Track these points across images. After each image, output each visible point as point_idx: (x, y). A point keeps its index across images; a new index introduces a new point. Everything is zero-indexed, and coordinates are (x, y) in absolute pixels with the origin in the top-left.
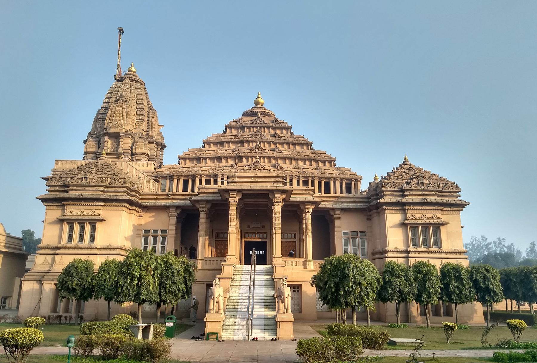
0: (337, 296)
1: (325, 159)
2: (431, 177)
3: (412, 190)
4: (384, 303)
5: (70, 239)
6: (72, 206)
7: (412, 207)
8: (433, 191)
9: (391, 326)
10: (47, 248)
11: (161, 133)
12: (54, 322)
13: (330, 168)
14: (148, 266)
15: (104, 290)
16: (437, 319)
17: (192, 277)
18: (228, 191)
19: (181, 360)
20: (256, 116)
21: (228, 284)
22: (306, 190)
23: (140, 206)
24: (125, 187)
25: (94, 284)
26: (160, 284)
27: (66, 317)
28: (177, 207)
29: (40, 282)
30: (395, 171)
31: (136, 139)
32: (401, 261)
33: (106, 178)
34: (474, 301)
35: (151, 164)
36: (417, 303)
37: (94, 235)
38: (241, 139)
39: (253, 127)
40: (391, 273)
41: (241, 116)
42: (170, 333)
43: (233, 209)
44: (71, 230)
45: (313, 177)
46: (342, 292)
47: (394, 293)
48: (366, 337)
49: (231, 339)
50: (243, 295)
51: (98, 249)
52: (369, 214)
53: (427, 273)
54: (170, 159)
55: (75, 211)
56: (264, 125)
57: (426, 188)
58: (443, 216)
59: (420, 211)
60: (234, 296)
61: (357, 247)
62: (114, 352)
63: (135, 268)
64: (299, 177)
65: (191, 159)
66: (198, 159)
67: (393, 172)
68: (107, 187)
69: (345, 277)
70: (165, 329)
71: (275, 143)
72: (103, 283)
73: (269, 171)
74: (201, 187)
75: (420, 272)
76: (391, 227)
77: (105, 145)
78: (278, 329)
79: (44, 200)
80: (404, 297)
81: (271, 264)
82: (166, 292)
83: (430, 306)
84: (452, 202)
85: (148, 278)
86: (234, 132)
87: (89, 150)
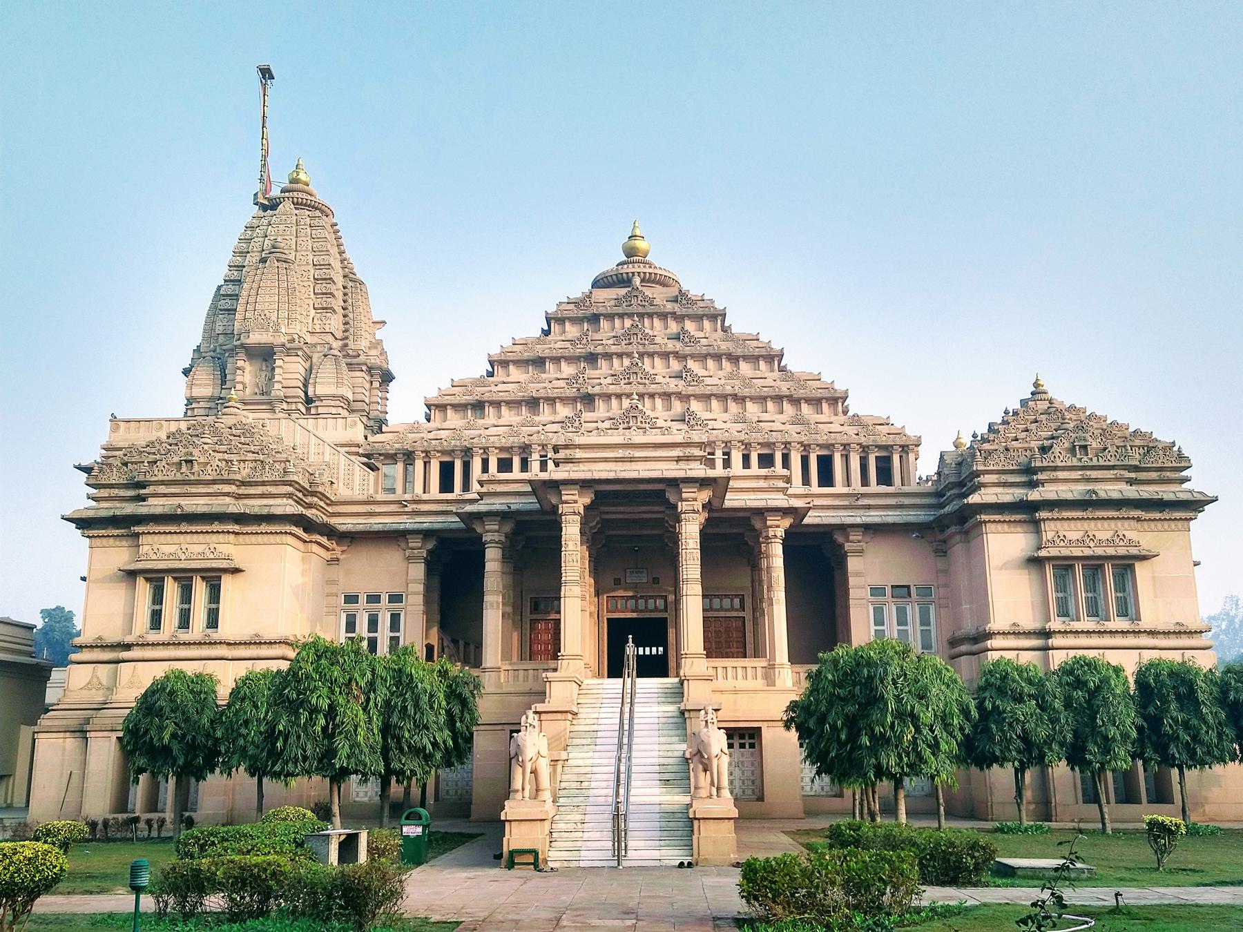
1: (819, 394)
2: (1109, 430)
3: (1055, 469)
4: (982, 769)
5: (156, 621)
6: (156, 537)
7: (1056, 514)
8: (1113, 467)
10: (97, 647)
11: (380, 342)
12: (119, 836)
13: (833, 419)
14: (350, 680)
15: (244, 749)
16: (1129, 809)
17: (471, 712)
19: (435, 918)
20: (629, 288)
21: (562, 725)
22: (766, 478)
24: (289, 483)
25: (219, 734)
26: (386, 729)
27: (149, 822)
28: (427, 534)
29: (82, 732)
30: (1010, 419)
32: (1026, 658)
34: (1233, 760)
35: (355, 423)
36: (1072, 769)
37: (218, 609)
38: (591, 348)
39: (622, 316)
41: (587, 287)
42: (416, 854)
43: (571, 531)
44: (158, 598)
46: (865, 740)
47: (1009, 741)
49: (573, 864)
51: (229, 644)
52: (940, 537)
54: (404, 409)
55: (163, 549)
56: (650, 309)
57: (1095, 462)
58: (1139, 535)
59: (1079, 523)
60: (578, 757)
61: (909, 628)
62: (260, 902)
64: (747, 445)
65: (459, 407)
66: (479, 406)
67: (1005, 422)
68: (243, 483)
69: (874, 701)
70: (400, 842)
73: (665, 430)
74: (485, 477)
75: (1080, 684)
76: (1004, 567)
77: (239, 379)
78: (695, 837)
80: (1035, 753)
81: (678, 675)
82: (401, 750)
83: (1109, 775)
84: (1166, 497)
85: (352, 711)
86: (572, 331)
87: (197, 392)
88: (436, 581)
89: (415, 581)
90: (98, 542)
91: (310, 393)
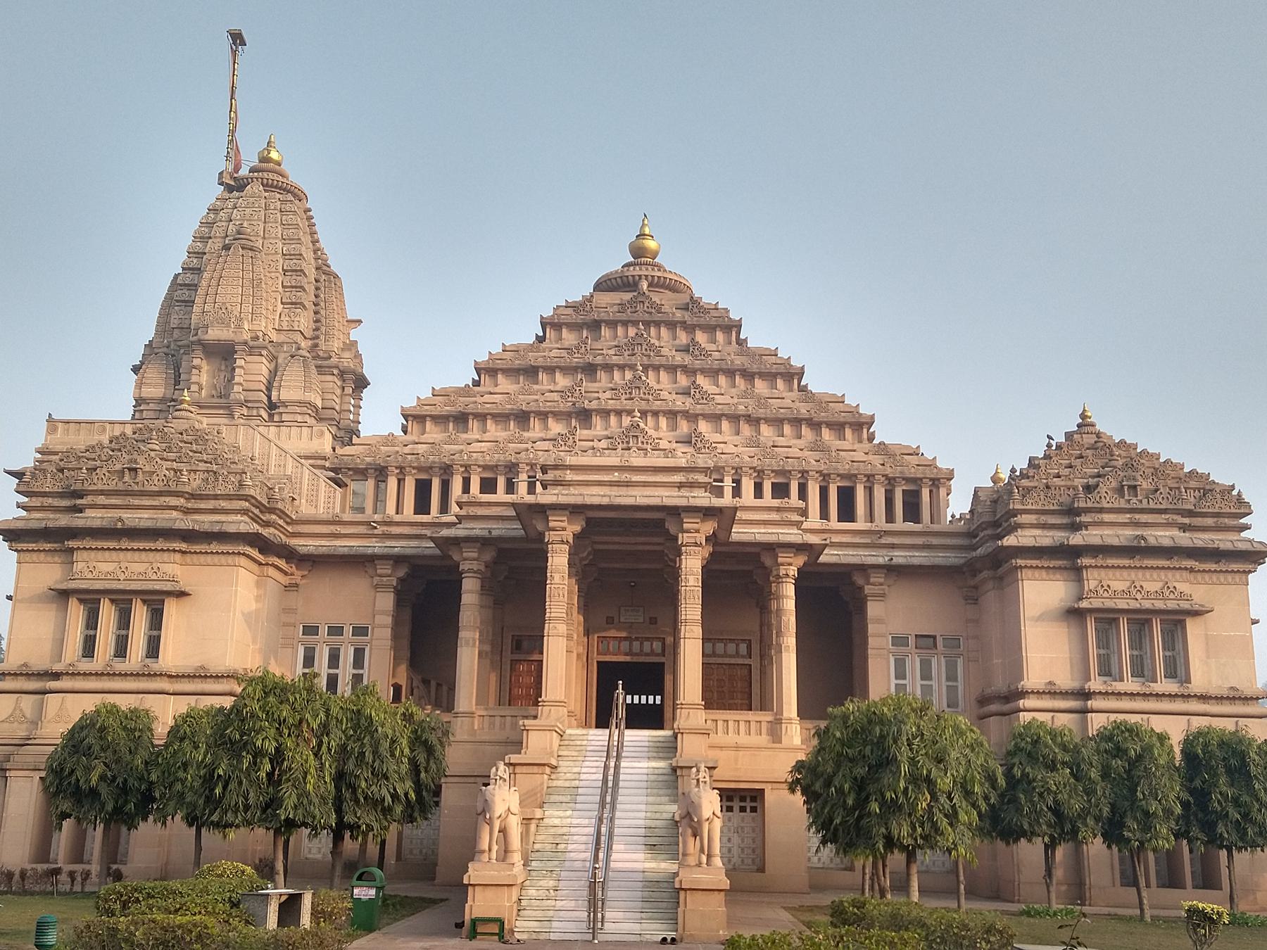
0: (860, 817)
2: (1163, 470)
3: (1101, 510)
4: (1008, 844)
5: (89, 648)
6: (93, 554)
7: (1100, 562)
8: (1165, 511)
9: (1028, 913)
10: (21, 674)
12: (37, 889)
13: (856, 446)
14: (301, 722)
15: (181, 795)
18: (542, 510)
22: (778, 509)
23: (290, 554)
24: (246, 498)
25: (154, 777)
26: (340, 777)
27: (72, 875)
28: (398, 560)
31: (280, 361)
32: (1063, 720)
33: (190, 471)
35: (322, 433)
36: (1109, 847)
37: (159, 637)
39: (625, 324)
40: (1029, 755)
43: (559, 561)
44: (92, 622)
45: (804, 473)
46: (875, 807)
47: (1039, 814)
48: (942, 938)
50: (578, 812)
51: (170, 676)
53: (1140, 757)
55: (101, 567)
56: (658, 317)
57: (1145, 504)
58: (1191, 588)
61: (934, 683)
63: (262, 729)
64: (760, 473)
65: (440, 420)
66: (461, 419)
69: (886, 762)
71: (690, 372)
72: (181, 774)
74: (465, 498)
75: (1119, 751)
76: (1040, 618)
77: (194, 379)
79: (13, 535)
80: (1068, 827)
82: (357, 801)
83: (1151, 855)
84: (1223, 546)
85: (301, 756)
86: (569, 337)
87: (148, 392)
88: (407, 615)
89: (383, 613)
90: (27, 557)
91: (274, 398)
